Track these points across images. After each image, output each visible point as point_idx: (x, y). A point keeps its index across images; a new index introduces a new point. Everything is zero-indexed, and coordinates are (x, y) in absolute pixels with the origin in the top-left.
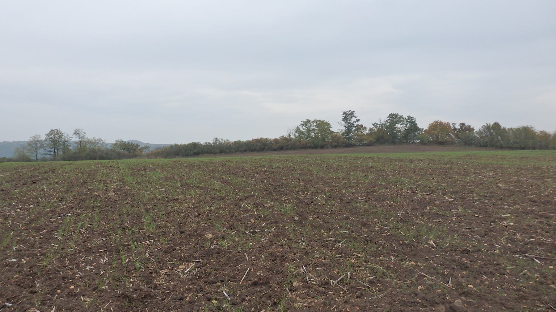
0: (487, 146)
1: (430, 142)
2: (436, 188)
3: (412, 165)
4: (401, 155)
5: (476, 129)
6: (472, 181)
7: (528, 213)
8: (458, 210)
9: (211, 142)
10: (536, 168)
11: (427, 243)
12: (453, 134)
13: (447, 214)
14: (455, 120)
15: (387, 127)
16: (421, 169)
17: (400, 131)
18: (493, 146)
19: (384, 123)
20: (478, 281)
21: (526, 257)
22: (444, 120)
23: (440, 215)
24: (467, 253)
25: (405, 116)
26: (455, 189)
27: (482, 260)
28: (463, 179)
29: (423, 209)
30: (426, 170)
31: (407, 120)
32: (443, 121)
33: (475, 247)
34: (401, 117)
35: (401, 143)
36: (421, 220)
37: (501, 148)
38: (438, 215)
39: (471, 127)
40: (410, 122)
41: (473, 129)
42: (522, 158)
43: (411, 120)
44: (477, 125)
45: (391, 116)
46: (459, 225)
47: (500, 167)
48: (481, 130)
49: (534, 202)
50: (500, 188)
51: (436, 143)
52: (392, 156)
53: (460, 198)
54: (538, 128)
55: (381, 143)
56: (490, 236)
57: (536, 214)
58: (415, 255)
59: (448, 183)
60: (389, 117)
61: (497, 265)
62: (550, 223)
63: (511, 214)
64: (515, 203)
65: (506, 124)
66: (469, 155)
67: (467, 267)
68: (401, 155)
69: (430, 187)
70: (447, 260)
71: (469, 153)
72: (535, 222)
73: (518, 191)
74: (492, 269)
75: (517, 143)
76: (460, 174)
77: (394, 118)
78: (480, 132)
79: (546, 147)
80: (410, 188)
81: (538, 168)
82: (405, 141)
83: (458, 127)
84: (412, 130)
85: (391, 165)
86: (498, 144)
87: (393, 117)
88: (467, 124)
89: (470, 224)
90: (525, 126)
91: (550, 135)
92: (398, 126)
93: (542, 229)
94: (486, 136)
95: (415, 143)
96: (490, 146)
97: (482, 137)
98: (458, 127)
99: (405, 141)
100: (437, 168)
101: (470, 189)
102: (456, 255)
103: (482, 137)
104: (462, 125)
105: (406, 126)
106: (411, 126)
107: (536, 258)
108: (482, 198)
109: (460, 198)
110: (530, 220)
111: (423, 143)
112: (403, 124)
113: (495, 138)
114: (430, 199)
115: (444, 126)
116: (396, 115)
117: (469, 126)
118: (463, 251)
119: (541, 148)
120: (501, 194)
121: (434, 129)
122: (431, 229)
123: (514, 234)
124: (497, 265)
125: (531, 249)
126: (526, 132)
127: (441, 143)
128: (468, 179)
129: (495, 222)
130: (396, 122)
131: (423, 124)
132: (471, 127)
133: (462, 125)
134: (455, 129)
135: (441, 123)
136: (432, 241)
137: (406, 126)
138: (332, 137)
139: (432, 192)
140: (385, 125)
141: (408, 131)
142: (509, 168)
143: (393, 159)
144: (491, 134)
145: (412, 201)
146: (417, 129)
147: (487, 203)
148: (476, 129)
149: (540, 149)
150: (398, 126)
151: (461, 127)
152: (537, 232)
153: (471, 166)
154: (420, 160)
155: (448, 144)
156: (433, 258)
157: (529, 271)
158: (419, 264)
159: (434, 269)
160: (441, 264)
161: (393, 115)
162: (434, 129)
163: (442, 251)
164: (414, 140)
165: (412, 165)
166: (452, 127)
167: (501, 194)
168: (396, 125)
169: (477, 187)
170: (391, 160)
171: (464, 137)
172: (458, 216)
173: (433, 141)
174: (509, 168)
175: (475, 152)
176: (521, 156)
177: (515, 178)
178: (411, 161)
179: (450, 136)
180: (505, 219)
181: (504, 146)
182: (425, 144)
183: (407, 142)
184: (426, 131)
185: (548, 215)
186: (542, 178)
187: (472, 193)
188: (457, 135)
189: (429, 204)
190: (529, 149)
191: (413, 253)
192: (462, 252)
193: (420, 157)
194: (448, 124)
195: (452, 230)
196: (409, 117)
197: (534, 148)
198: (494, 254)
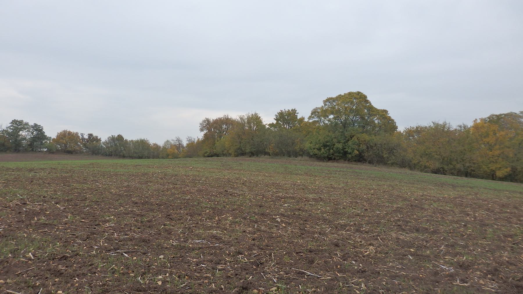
0: (112, 155)
1: (58, 151)
2: (50, 197)
3: (31, 175)
4: (21, 164)
5: (103, 140)
6: (88, 188)
7: (128, 214)
8: (67, 217)
9: (268, 119)
10: (144, 174)
11: (24, 257)
12: (81, 144)
13: (55, 222)
14: (83, 130)
15: (8, 133)
16: (40, 178)
17: (25, 139)
18: (117, 155)
19: (5, 129)
20: (69, 285)
21: (117, 253)
22: (73, 130)
23: (47, 224)
24: (65, 259)
25: (31, 123)
26: (70, 197)
27: (79, 263)
28: (80, 187)
29: (30, 220)
30: (45, 179)
31: (33, 127)
32: (72, 131)
33: (75, 251)
34: (27, 124)
35: (26, 151)
36: (25, 232)
37: (124, 157)
38: (45, 225)
39: (99, 138)
40: (36, 130)
41: (100, 140)
42: (137, 166)
43: (37, 128)
44: (104, 136)
45: (14, 122)
46: (64, 232)
47: (116, 175)
48: (107, 141)
49: (136, 203)
50: (111, 193)
51: (65, 152)
52: (12, 165)
53: (73, 206)
54: (152, 141)
55: (96, 154)
56: (91, 239)
57: (134, 214)
58: (7, 272)
59: (64, 191)
60: (12, 123)
61: (91, 265)
62: (143, 220)
63: (115, 216)
64: (121, 205)
65: (128, 137)
66: (93, 164)
67: (61, 274)
68: (21, 164)
69: (44, 197)
70: (42, 270)
71: (94, 161)
72: (132, 221)
73: (126, 195)
74: (85, 270)
75: (136, 153)
76: (78, 182)
77: (18, 125)
78: (106, 143)
79: (157, 157)
80: (22, 199)
81: (146, 174)
82: (30, 149)
83: (86, 137)
84: (38, 138)
85: (6, 175)
86: (121, 154)
87: (16, 124)
88: (94, 135)
89: (75, 230)
90: (143, 139)
91: (160, 147)
92: (23, 133)
93: (136, 226)
94: (112, 146)
95: (42, 152)
96: (114, 155)
97: (108, 147)
98: (86, 137)
99: (30, 149)
100: (57, 177)
101: (84, 196)
102: (54, 263)
103: (108, 147)
104: (90, 135)
105: (32, 133)
106: (37, 134)
107: (125, 252)
108: (93, 203)
109: (73, 206)
110: (129, 220)
111: (50, 151)
112: (29, 131)
113: (118, 148)
114: (40, 209)
115: (72, 135)
116: (21, 122)
117: (97, 137)
118: (61, 258)
119: (154, 157)
120: (111, 199)
121: (62, 139)
122: (33, 241)
123: (113, 234)
124: (91, 265)
125: (123, 245)
126: (143, 143)
127: (70, 152)
128: (86, 186)
129: (99, 224)
130: (21, 129)
131: (51, 132)
132: (99, 138)
133: (90, 135)
134: (83, 139)
135: (70, 133)
136: (30, 254)
137: (32, 133)
138: (171, 146)
139: (45, 202)
140: (6, 131)
141: (34, 139)
142: (123, 175)
143: (10, 169)
144: (116, 145)
145: (20, 213)
146: (45, 137)
147: (96, 208)
148: (103, 140)
149: (153, 158)
150: (23, 133)
151: (89, 137)
152: (131, 229)
153: (91, 174)
154: (41, 169)
155: (77, 153)
156: (28, 271)
157: (116, 265)
158: (8, 281)
159: (26, 283)
160: (34, 277)
161: (17, 121)
162: (62, 139)
163: (39, 262)
164: (41, 148)
165: (31, 175)
166: (81, 137)
167: (111, 199)
168: (21, 132)
169: (92, 193)
170: (8, 169)
171: (91, 147)
172: (66, 224)
173: (62, 149)
174: (123, 175)
175: (99, 161)
176: (136, 164)
177: (126, 184)
178: (31, 170)
179: (78, 145)
180: (108, 221)
181: (126, 155)
182: (53, 153)
183: (33, 150)
184: (54, 139)
185: (144, 213)
186: (147, 182)
187: (86, 199)
188: (85, 145)
189: (38, 214)
190: (145, 158)
191: (6, 270)
192: (60, 259)
193: (42, 166)
194: (77, 134)
195: (57, 238)
196: (36, 125)
197: (149, 158)
198: (90, 256)
